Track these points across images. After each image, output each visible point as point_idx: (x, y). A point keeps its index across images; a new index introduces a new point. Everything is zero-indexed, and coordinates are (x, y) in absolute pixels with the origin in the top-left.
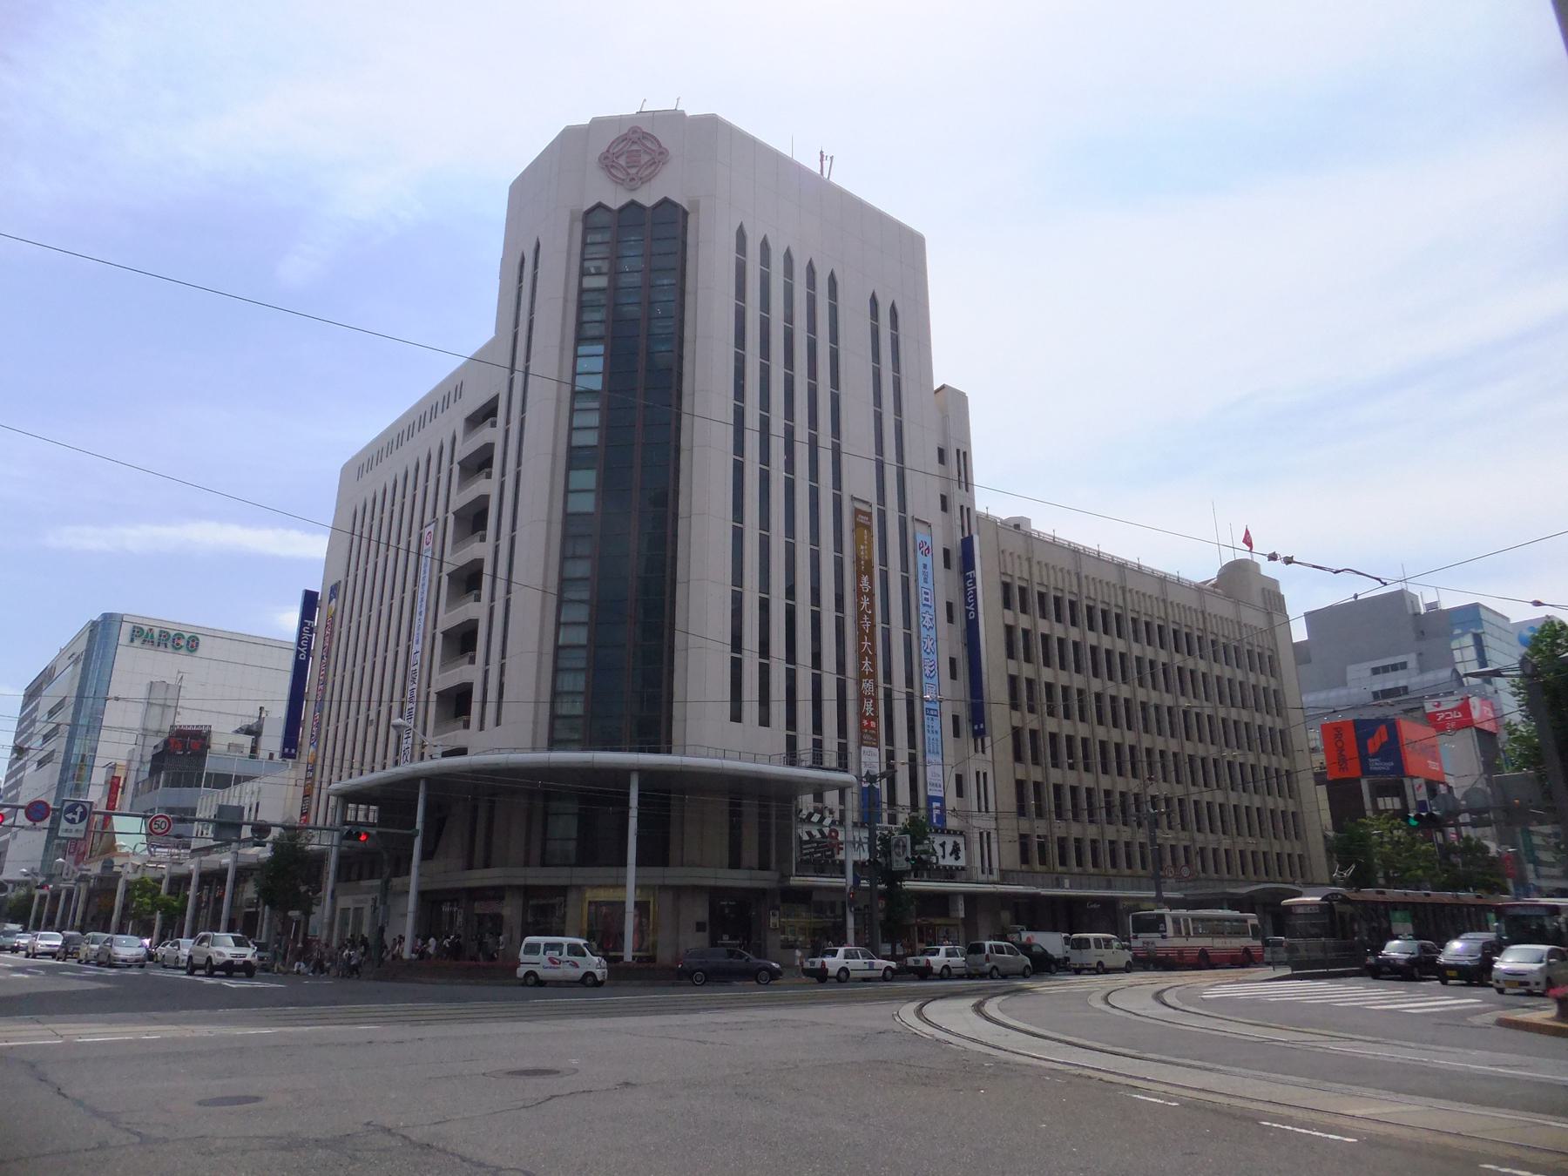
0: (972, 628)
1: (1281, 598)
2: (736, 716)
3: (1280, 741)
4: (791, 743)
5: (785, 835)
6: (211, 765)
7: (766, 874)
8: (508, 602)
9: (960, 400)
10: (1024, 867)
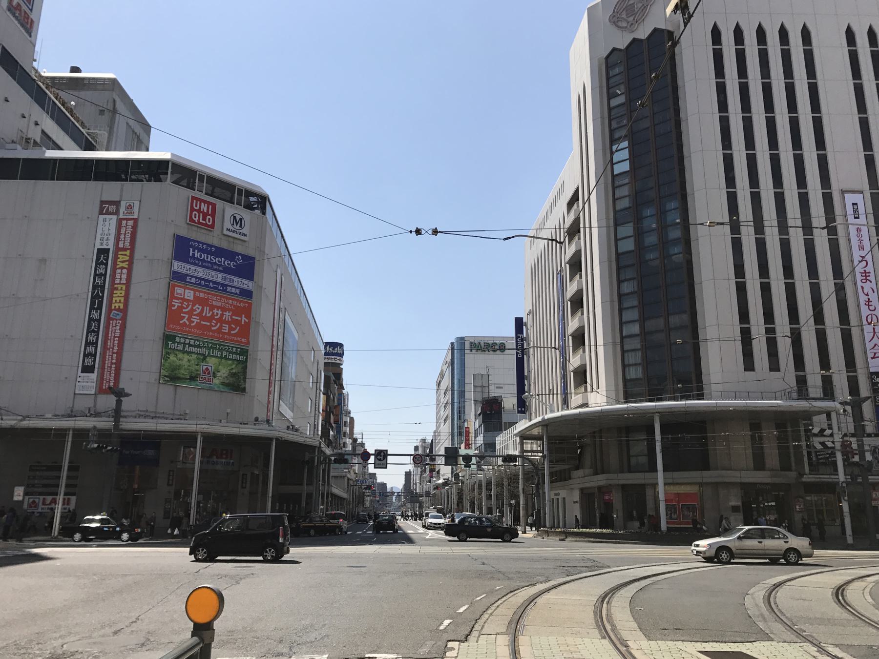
2: (749, 365)
4: (802, 382)
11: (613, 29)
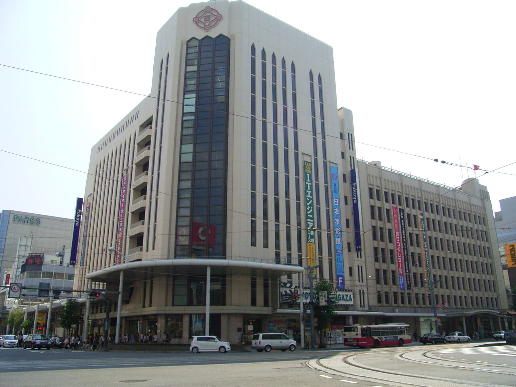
0: (355, 206)
1: (487, 194)
2: (253, 244)
3: (488, 252)
4: (278, 255)
5: (275, 293)
6: (44, 269)
7: (266, 308)
8: (157, 199)
9: (348, 113)
10: (380, 304)
11: (195, 26)
